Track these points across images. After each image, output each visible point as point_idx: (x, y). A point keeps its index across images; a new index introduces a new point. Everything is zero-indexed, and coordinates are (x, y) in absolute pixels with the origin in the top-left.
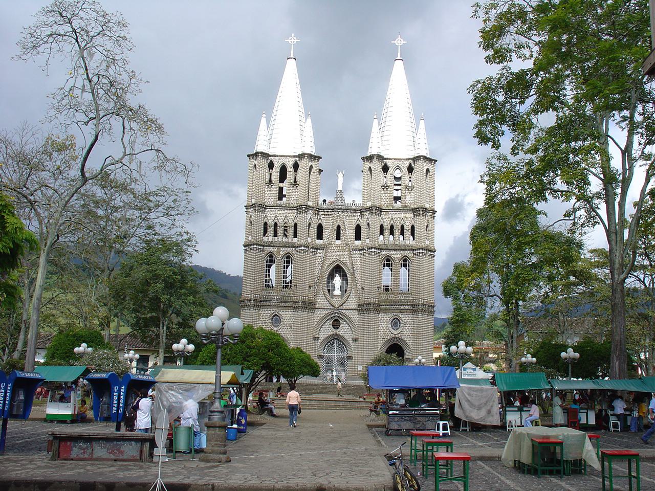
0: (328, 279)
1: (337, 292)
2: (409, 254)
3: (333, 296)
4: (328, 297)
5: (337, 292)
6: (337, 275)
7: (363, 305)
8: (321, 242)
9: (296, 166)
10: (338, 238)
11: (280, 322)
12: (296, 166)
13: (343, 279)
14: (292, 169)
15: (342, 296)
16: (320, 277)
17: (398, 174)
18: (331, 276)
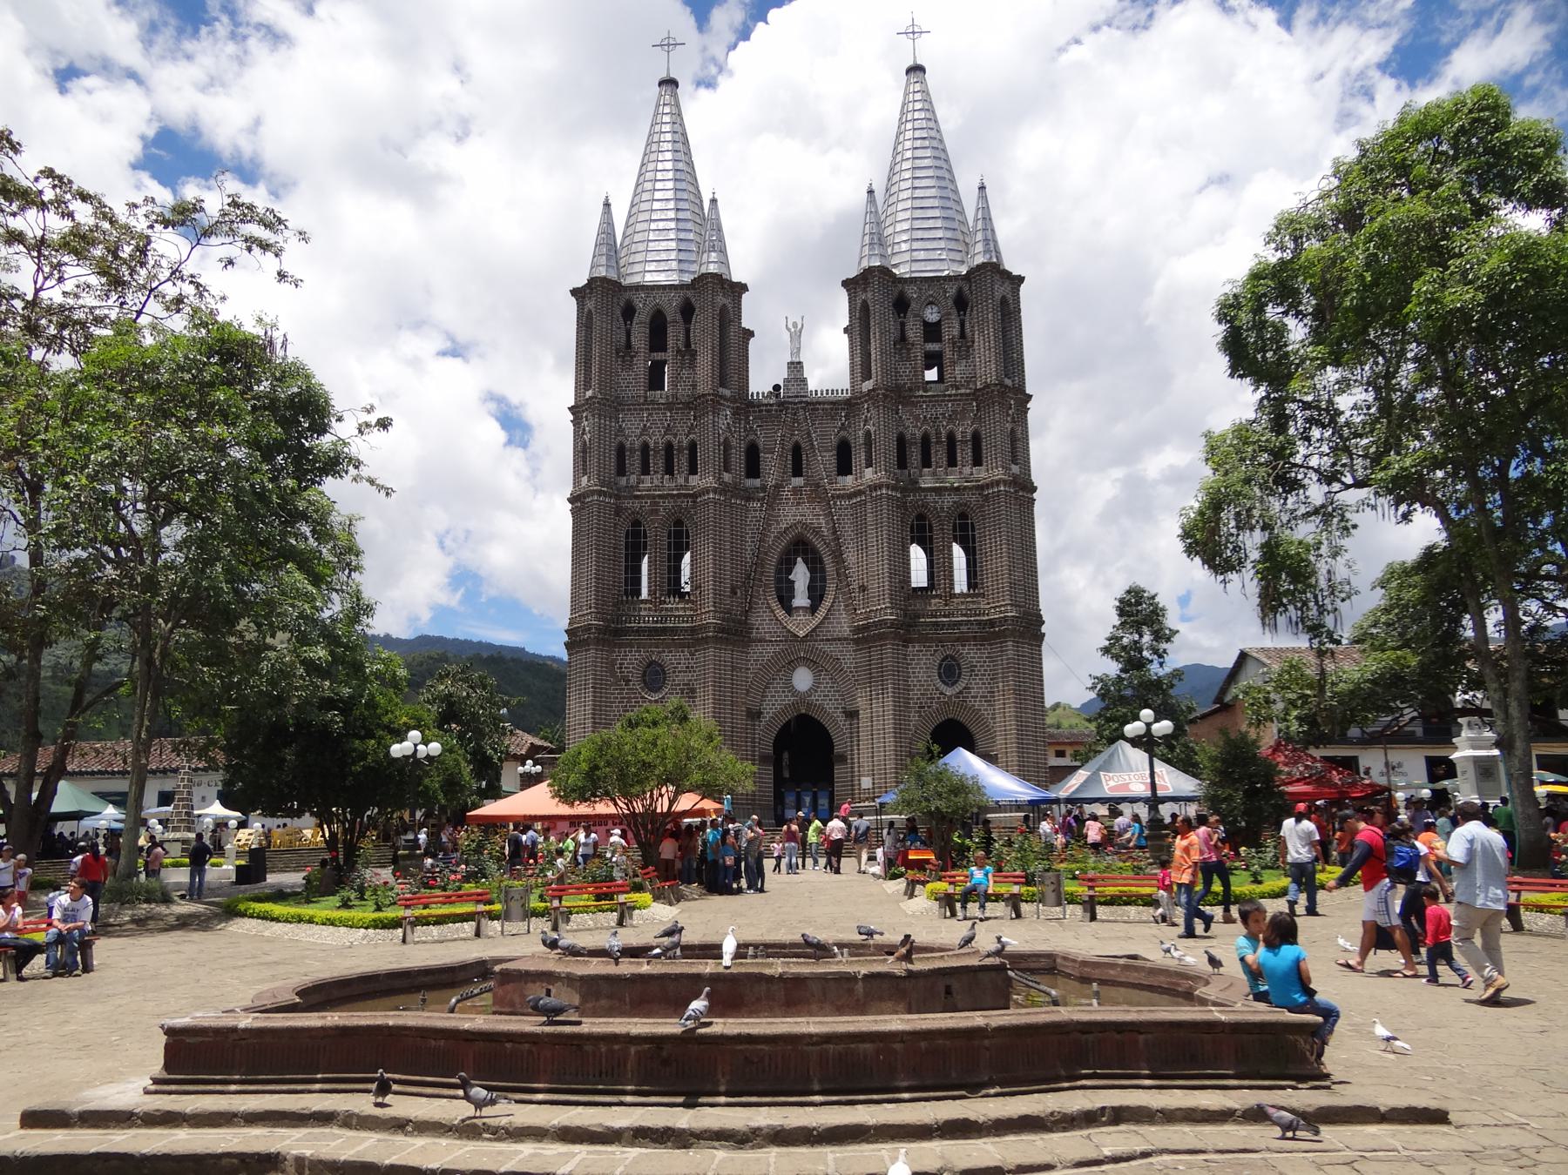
0: (779, 571)
1: (801, 600)
2: (973, 498)
3: (789, 610)
4: (781, 613)
5: (801, 600)
6: (799, 559)
7: (866, 627)
8: (757, 482)
9: (687, 311)
10: (797, 472)
11: (665, 679)
12: (687, 311)
13: (812, 570)
14: (679, 317)
15: (813, 609)
16: (759, 563)
17: (932, 315)
18: (787, 565)
